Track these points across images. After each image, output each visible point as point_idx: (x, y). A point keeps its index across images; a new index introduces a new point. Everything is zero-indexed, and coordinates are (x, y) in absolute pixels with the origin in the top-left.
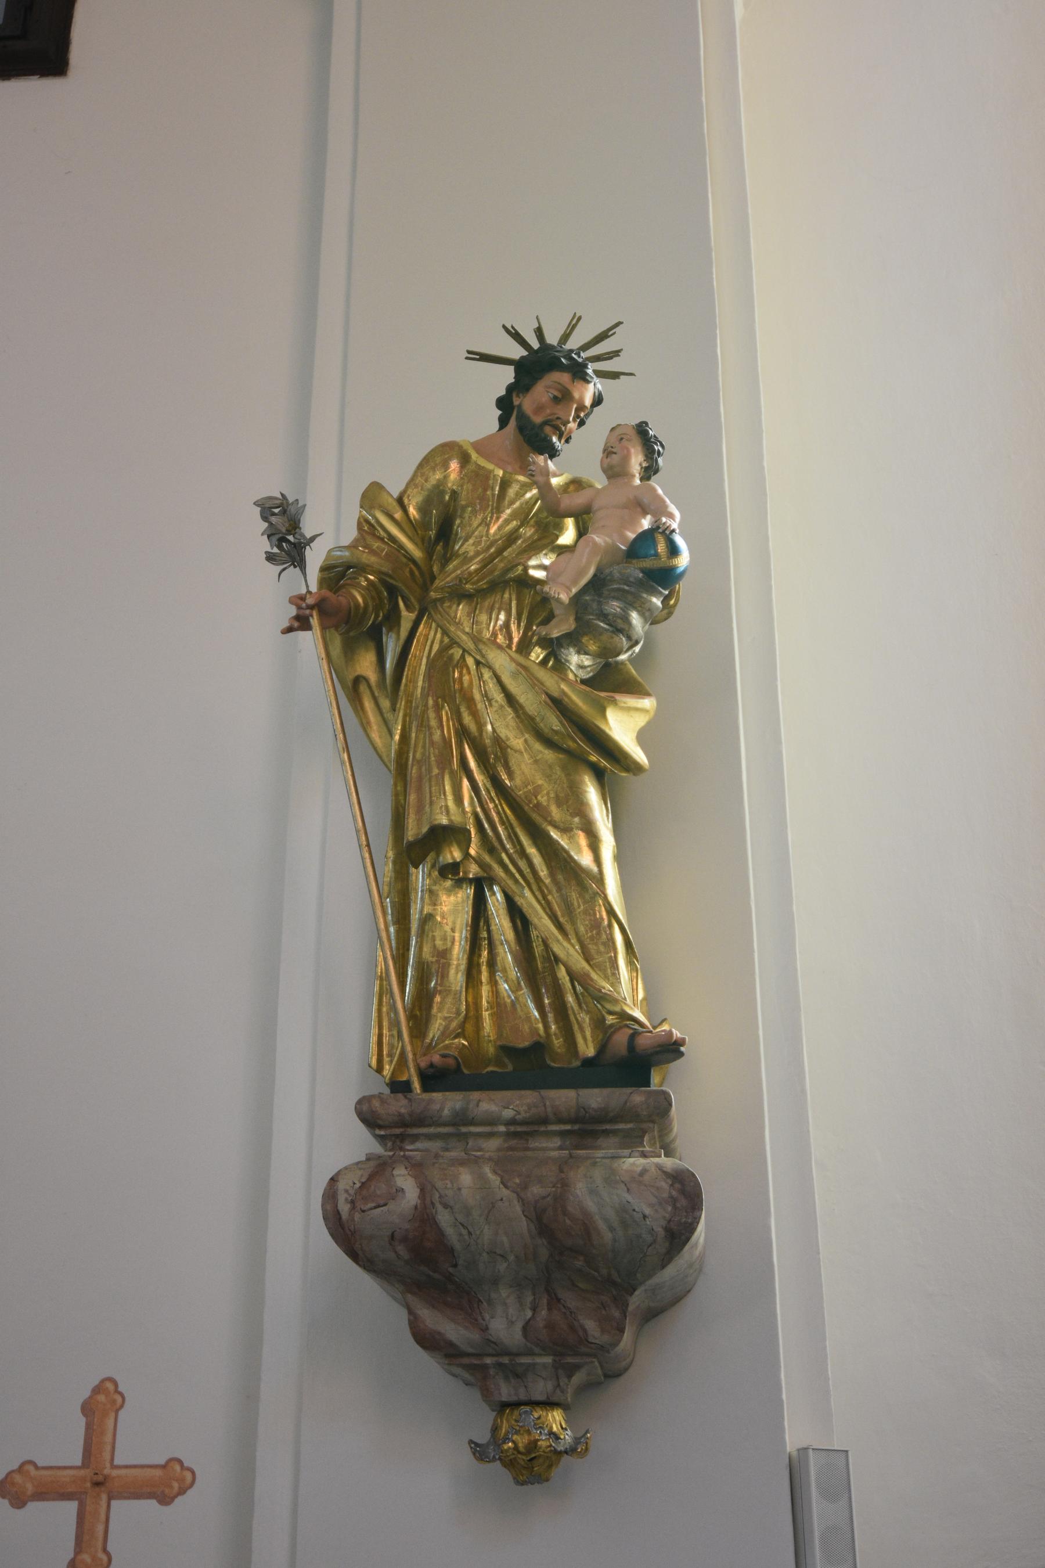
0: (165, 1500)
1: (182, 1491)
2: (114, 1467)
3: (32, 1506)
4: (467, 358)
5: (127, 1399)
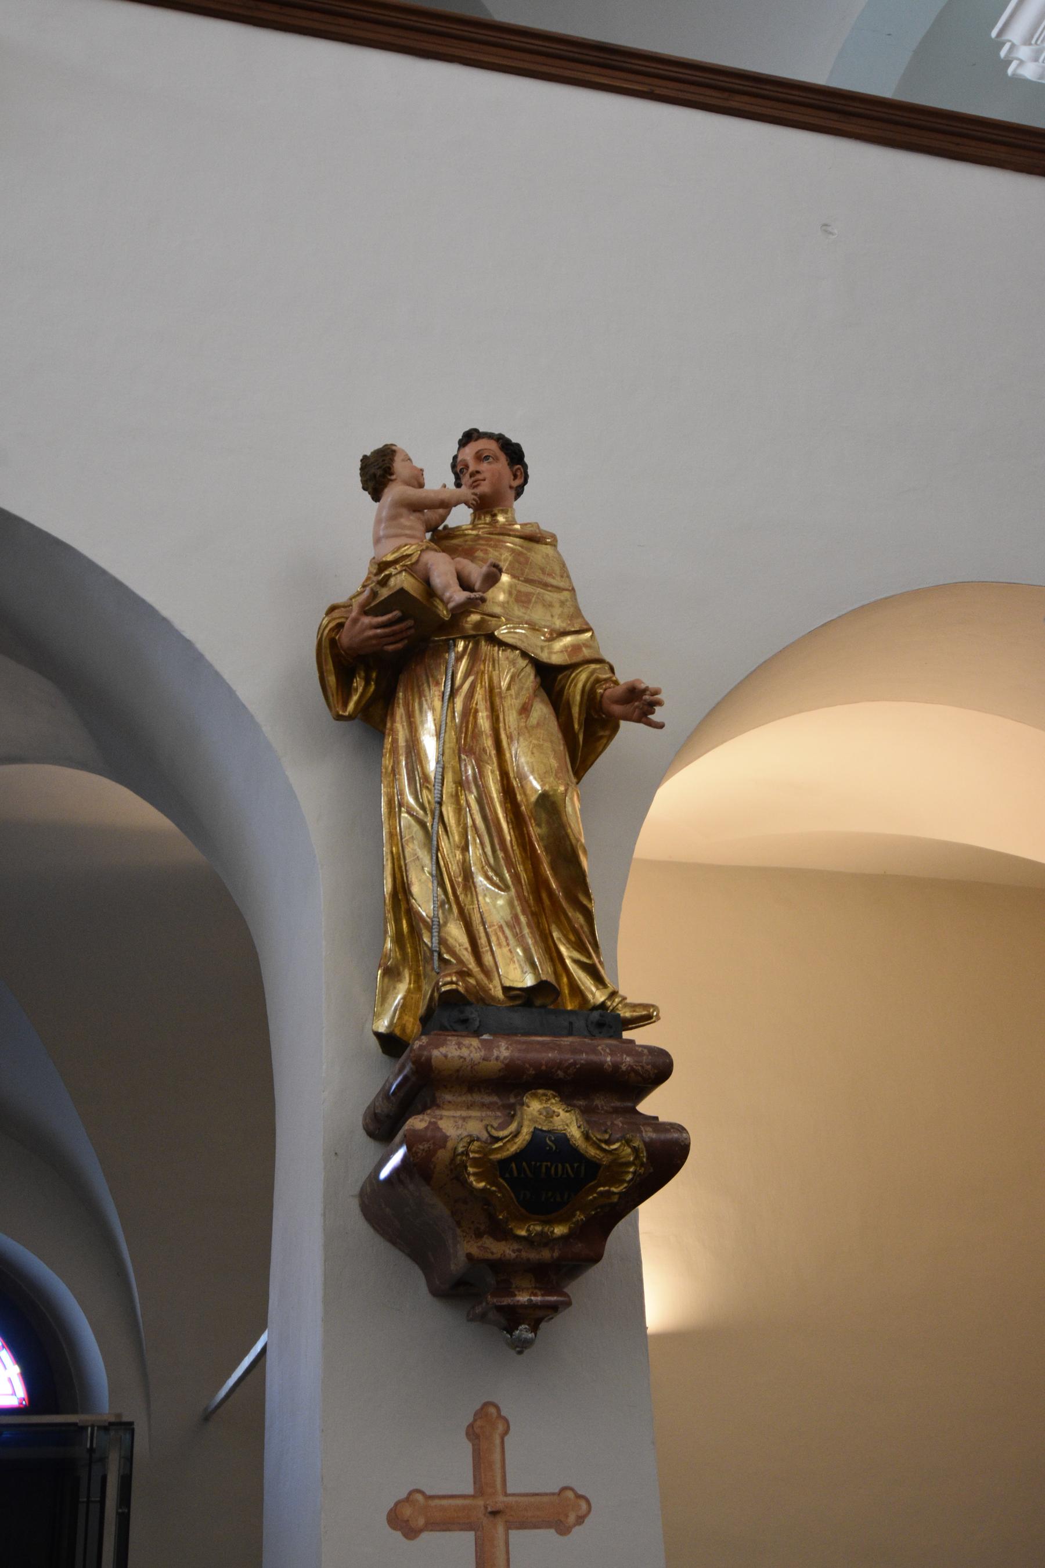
0: (563, 1529)
1: (580, 1520)
2: (506, 1495)
3: (425, 1536)
4: (10, 1380)
5: (588, 1496)
